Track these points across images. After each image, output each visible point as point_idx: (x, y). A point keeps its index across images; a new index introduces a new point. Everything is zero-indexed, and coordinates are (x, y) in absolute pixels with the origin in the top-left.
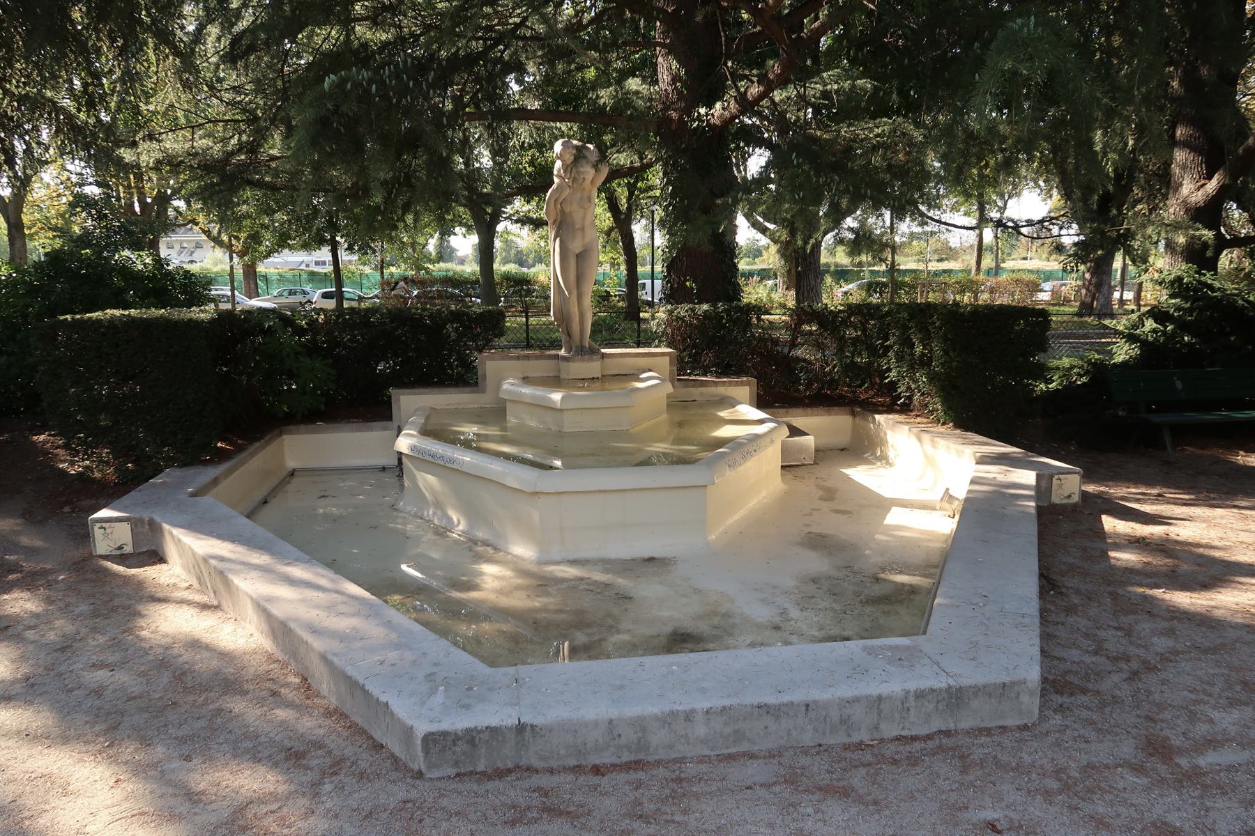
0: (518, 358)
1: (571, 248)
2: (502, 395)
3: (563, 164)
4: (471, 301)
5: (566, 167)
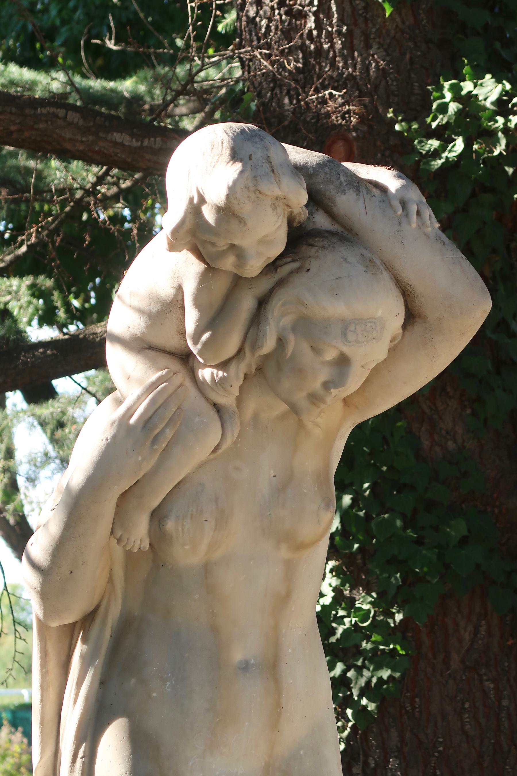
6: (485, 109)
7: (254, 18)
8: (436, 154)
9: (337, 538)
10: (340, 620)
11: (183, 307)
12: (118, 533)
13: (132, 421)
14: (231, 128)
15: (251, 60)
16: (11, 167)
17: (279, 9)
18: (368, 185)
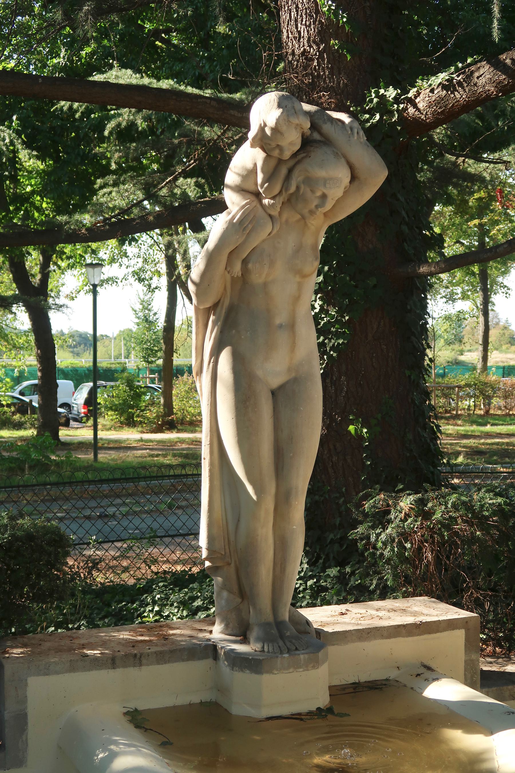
1: (259, 373)
6: (389, 101)
7: (291, 61)
8: (368, 121)
9: (322, 284)
10: (322, 319)
11: (256, 173)
12: (228, 269)
13: (235, 221)
14: (278, 94)
15: (289, 79)
16: (188, 129)
17: (302, 57)
18: (338, 122)
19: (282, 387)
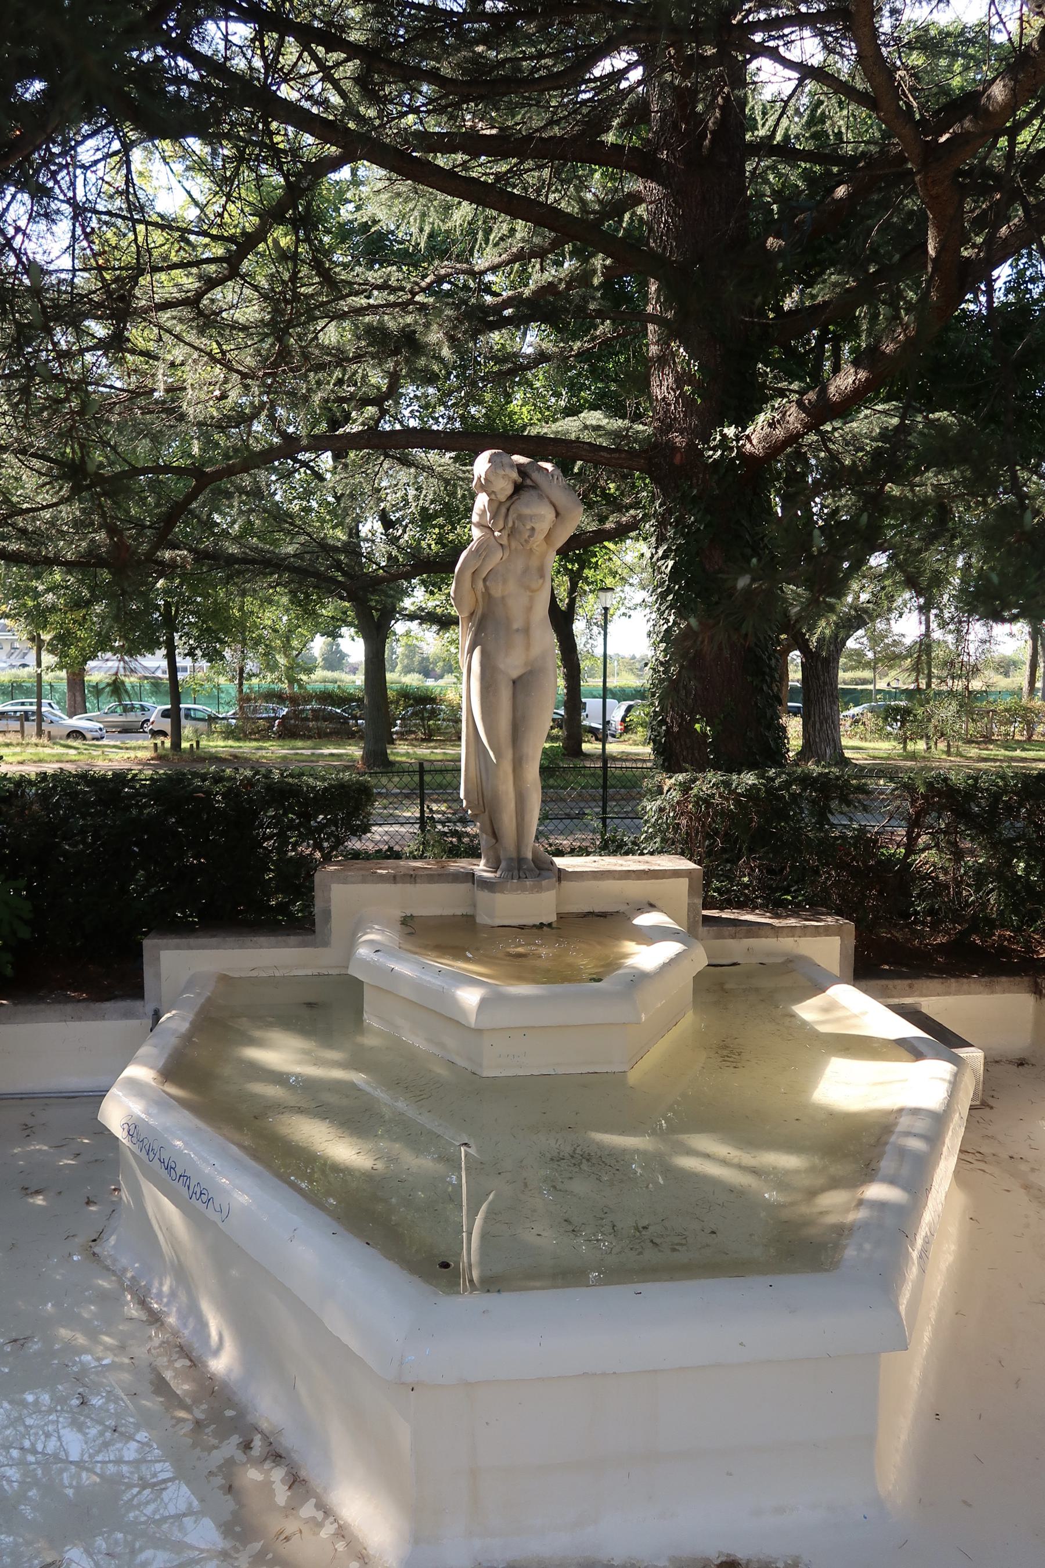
0: (394, 879)
1: (502, 666)
2: (354, 971)
3: (490, 501)
4: (357, 725)
5: (497, 508)
19: (520, 677)
